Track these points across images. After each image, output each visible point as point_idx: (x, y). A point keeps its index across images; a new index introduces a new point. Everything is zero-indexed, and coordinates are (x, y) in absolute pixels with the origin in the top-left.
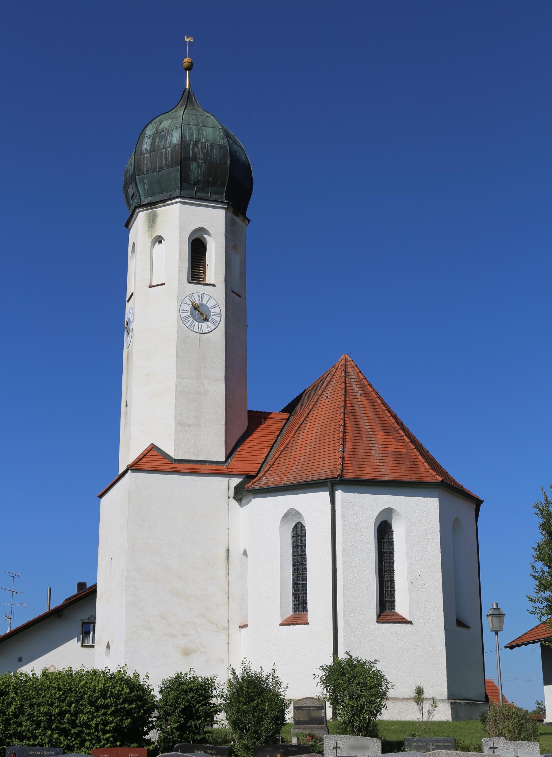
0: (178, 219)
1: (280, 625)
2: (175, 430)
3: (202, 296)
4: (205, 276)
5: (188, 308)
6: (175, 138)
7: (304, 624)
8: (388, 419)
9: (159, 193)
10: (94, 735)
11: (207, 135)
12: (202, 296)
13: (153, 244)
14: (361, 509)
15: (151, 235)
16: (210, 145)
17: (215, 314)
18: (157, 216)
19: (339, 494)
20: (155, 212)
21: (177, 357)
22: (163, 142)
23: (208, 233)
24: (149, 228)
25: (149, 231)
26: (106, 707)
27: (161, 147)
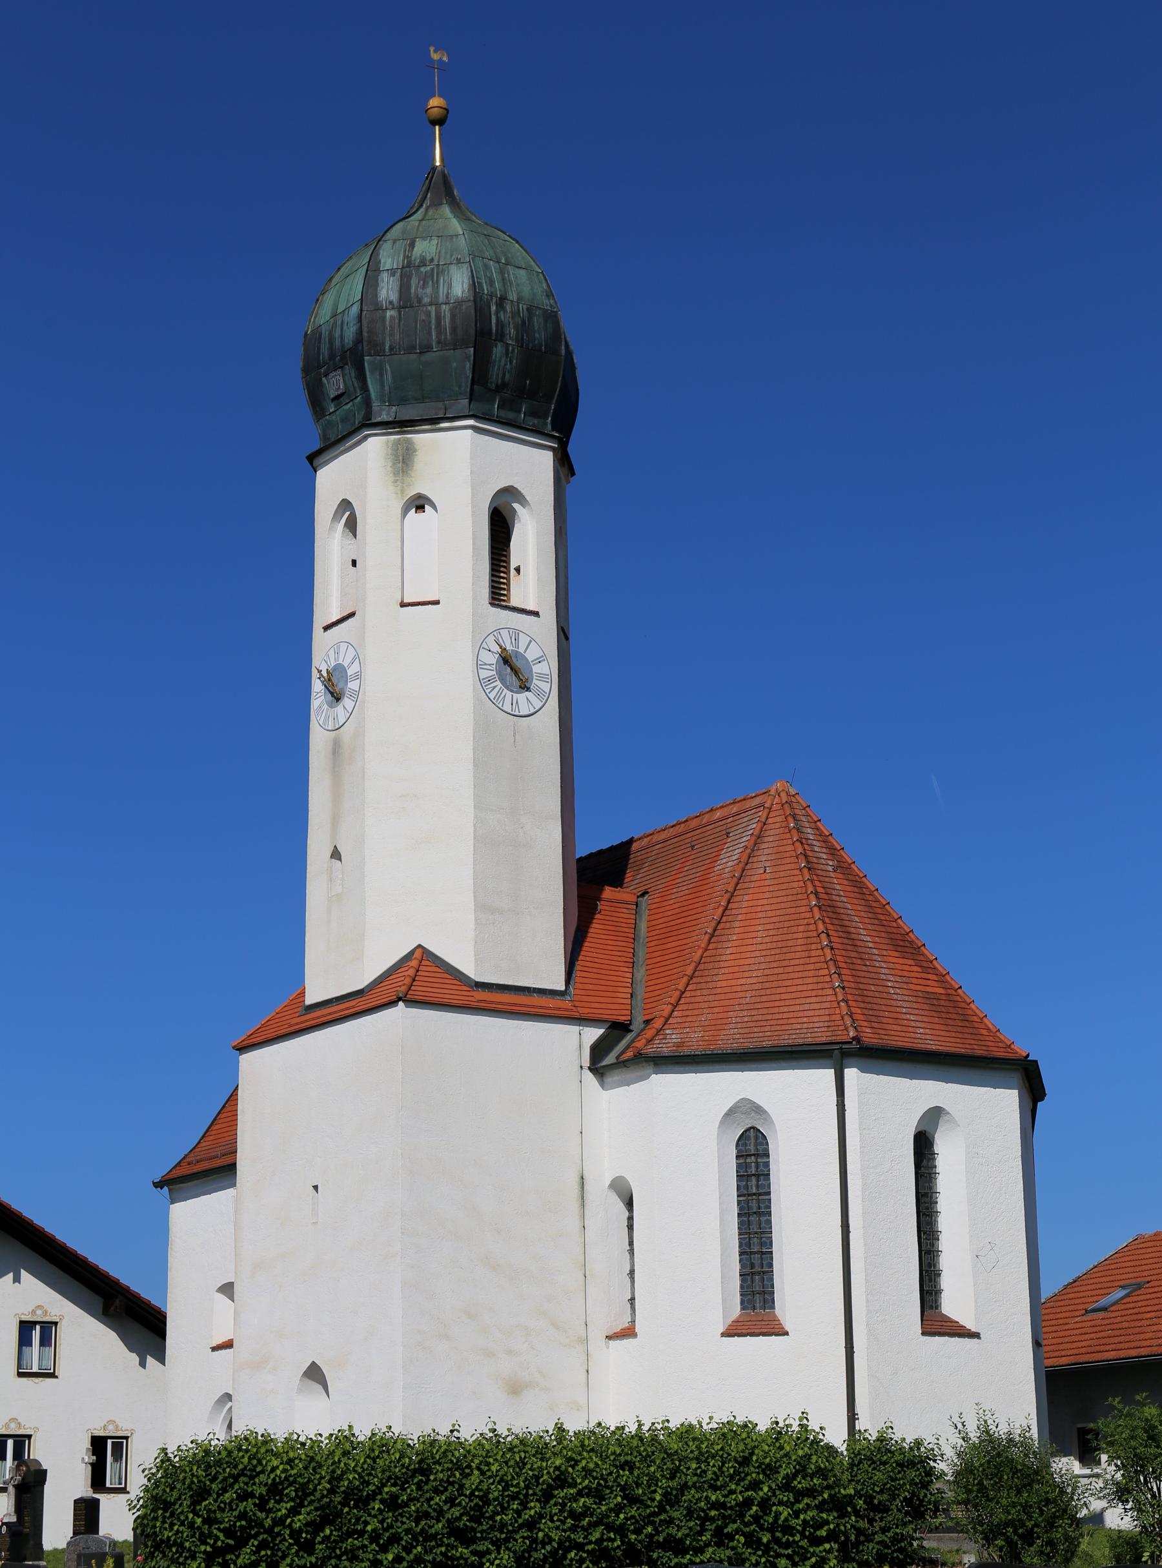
0: (465, 460)
1: (723, 1335)
2: (476, 920)
3: (516, 634)
4: (509, 590)
5: (492, 659)
6: (458, 284)
7: (777, 1335)
8: (894, 924)
9: (416, 399)
10: (798, 1546)
11: (518, 285)
12: (516, 634)
13: (405, 512)
14: (889, 1102)
15: (402, 491)
16: (528, 309)
17: (542, 677)
18: (415, 451)
19: (852, 1074)
20: (409, 442)
21: (475, 766)
22: (429, 290)
23: (522, 500)
24: (395, 474)
25: (396, 481)
26: (811, 1492)
27: (426, 300)
